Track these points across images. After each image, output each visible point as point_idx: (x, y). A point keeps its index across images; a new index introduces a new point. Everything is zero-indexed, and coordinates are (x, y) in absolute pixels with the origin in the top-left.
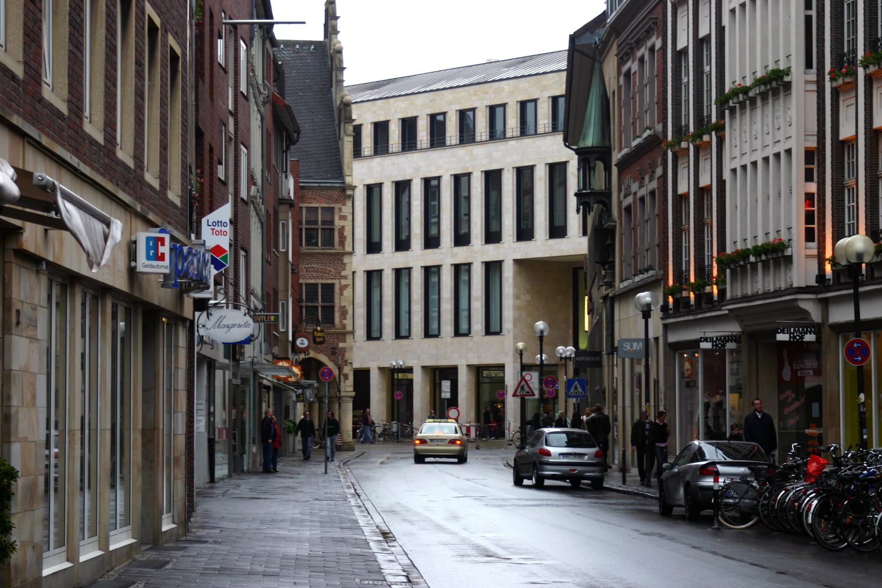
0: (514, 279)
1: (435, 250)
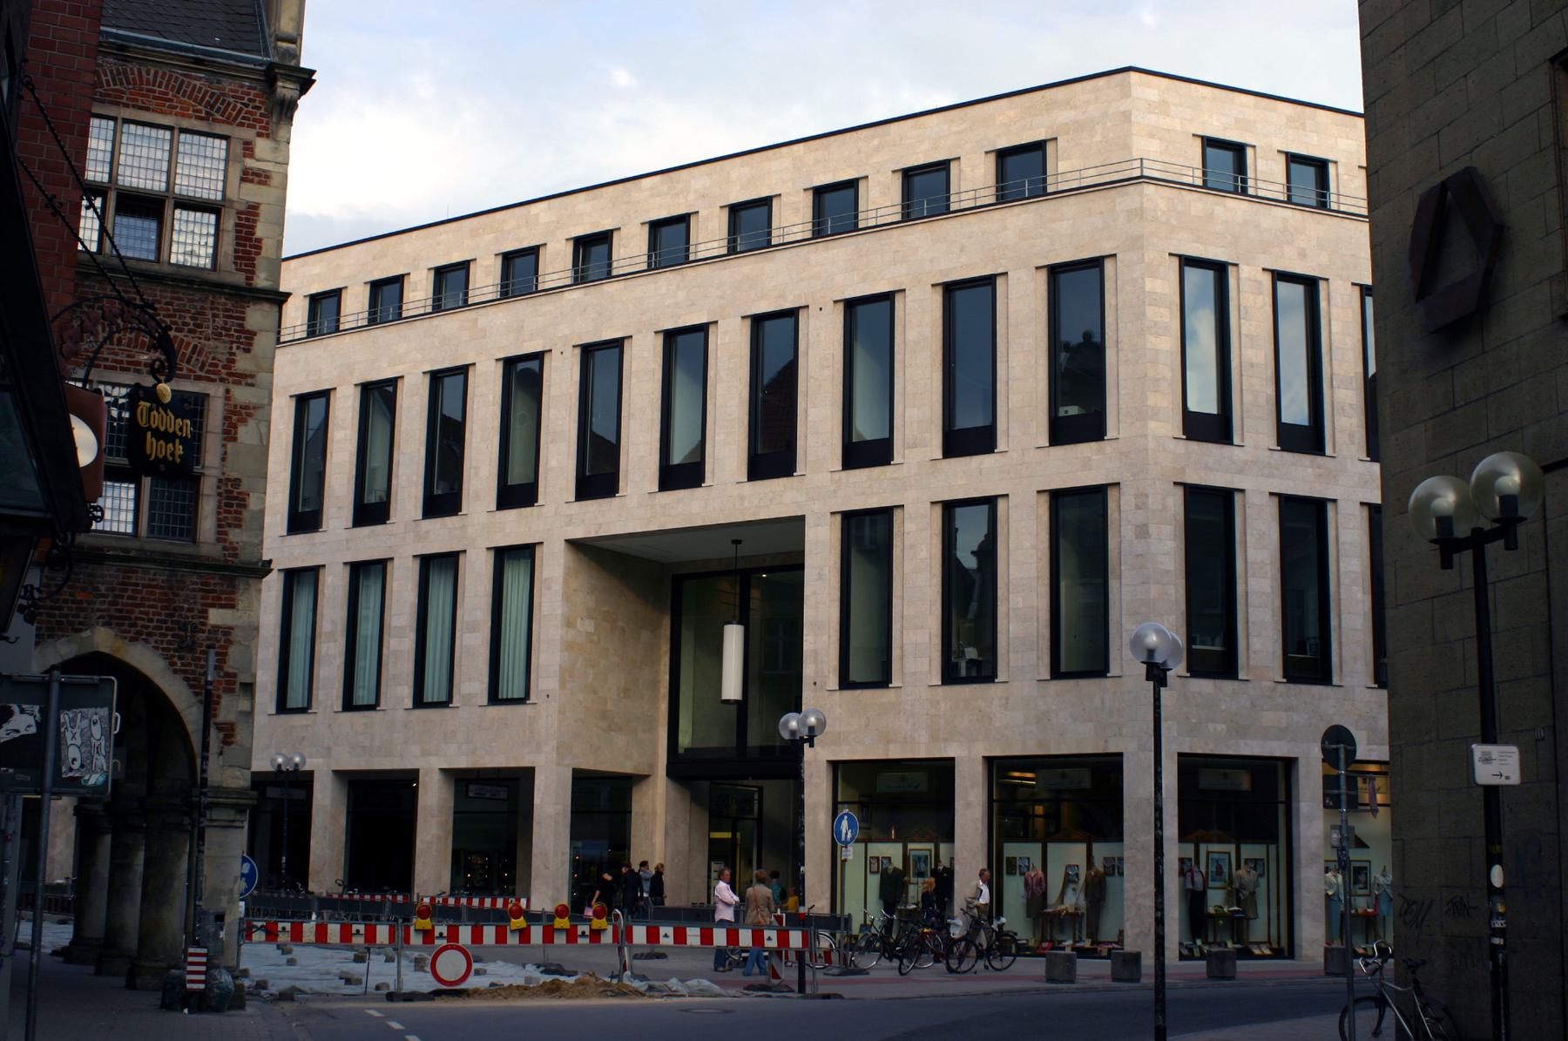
0: (566, 582)
1: (379, 528)
